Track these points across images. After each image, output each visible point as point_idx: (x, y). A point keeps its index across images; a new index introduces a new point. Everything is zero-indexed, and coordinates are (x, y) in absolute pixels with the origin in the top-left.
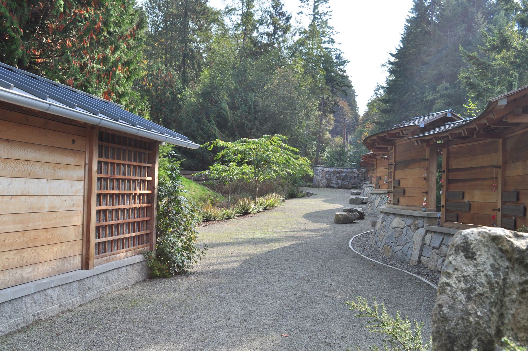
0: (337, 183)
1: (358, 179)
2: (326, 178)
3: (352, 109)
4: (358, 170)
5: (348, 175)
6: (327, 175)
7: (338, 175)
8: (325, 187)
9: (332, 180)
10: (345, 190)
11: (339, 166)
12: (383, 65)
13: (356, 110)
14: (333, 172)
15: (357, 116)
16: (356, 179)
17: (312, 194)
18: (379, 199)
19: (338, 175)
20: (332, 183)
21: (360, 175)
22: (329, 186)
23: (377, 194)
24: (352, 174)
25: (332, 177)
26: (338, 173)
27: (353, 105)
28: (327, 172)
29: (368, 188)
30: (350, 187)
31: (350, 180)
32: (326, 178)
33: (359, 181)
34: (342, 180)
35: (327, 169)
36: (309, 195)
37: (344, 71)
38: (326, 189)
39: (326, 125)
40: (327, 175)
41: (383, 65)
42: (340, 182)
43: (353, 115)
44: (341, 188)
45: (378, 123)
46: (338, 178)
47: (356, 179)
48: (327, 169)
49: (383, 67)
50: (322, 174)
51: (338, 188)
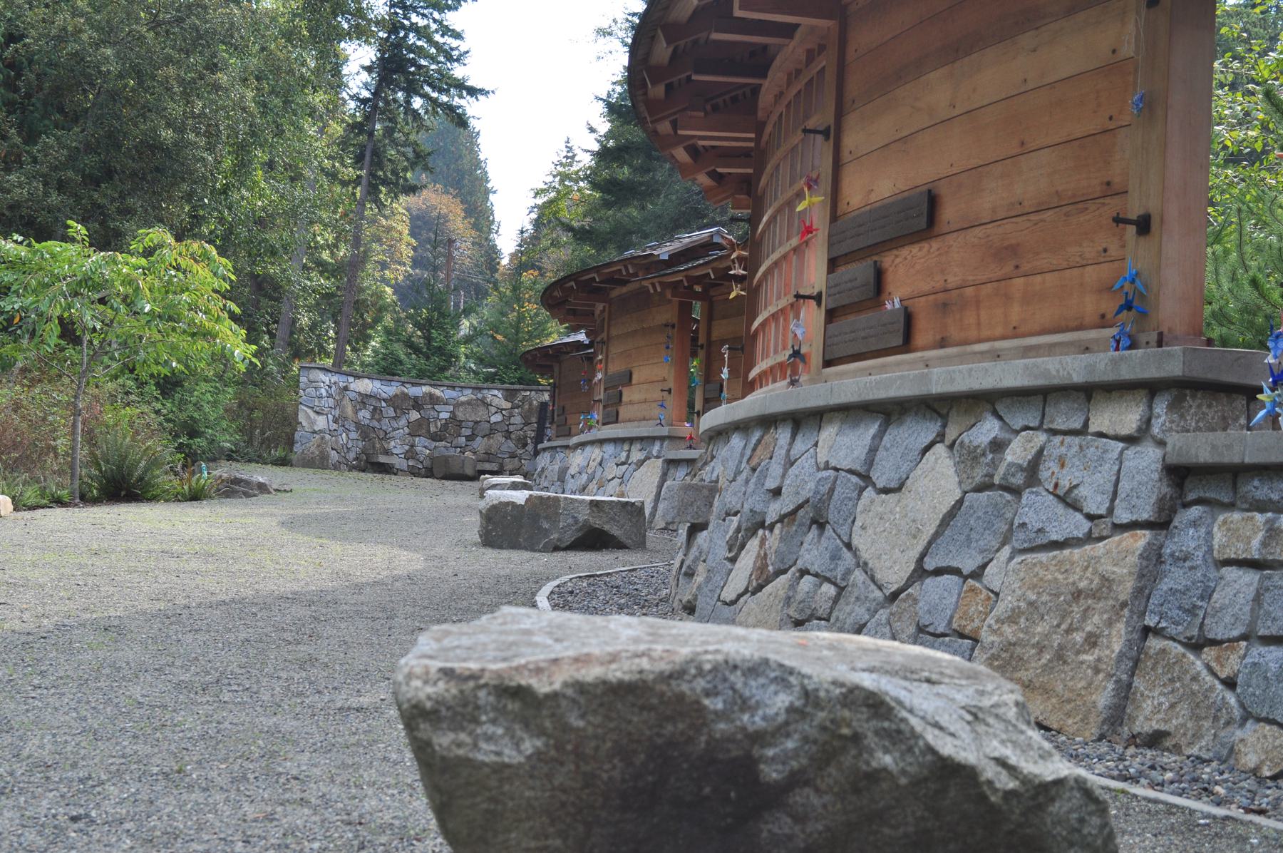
0: (411, 454)
1: (508, 434)
2: (358, 425)
3: (476, 226)
4: (510, 395)
5: (460, 415)
6: (364, 415)
7: (414, 415)
8: (352, 468)
9: (386, 437)
10: (448, 483)
11: (423, 376)
12: (604, 33)
13: (490, 231)
14: (391, 401)
15: (492, 254)
16: (499, 437)
17: (263, 488)
18: (939, 480)
19: (414, 415)
20: (387, 452)
21: (517, 419)
22: (372, 464)
23: (889, 412)
24: (481, 414)
25: (385, 424)
26: (417, 404)
27: (481, 217)
28: (364, 399)
29: (595, 453)
30: (469, 471)
31: (470, 438)
32: (358, 425)
33: (510, 446)
34: (435, 437)
35: (366, 386)
36: (234, 489)
37: (458, 36)
38: (355, 474)
39: (384, 266)
40: (364, 415)
41: (604, 33)
42: (423, 446)
43: (481, 246)
44: (430, 473)
45: (581, 235)
46: (416, 429)
47: (499, 437)
48: (366, 386)
49: (602, 40)
50: (338, 404)
51: (414, 472)
